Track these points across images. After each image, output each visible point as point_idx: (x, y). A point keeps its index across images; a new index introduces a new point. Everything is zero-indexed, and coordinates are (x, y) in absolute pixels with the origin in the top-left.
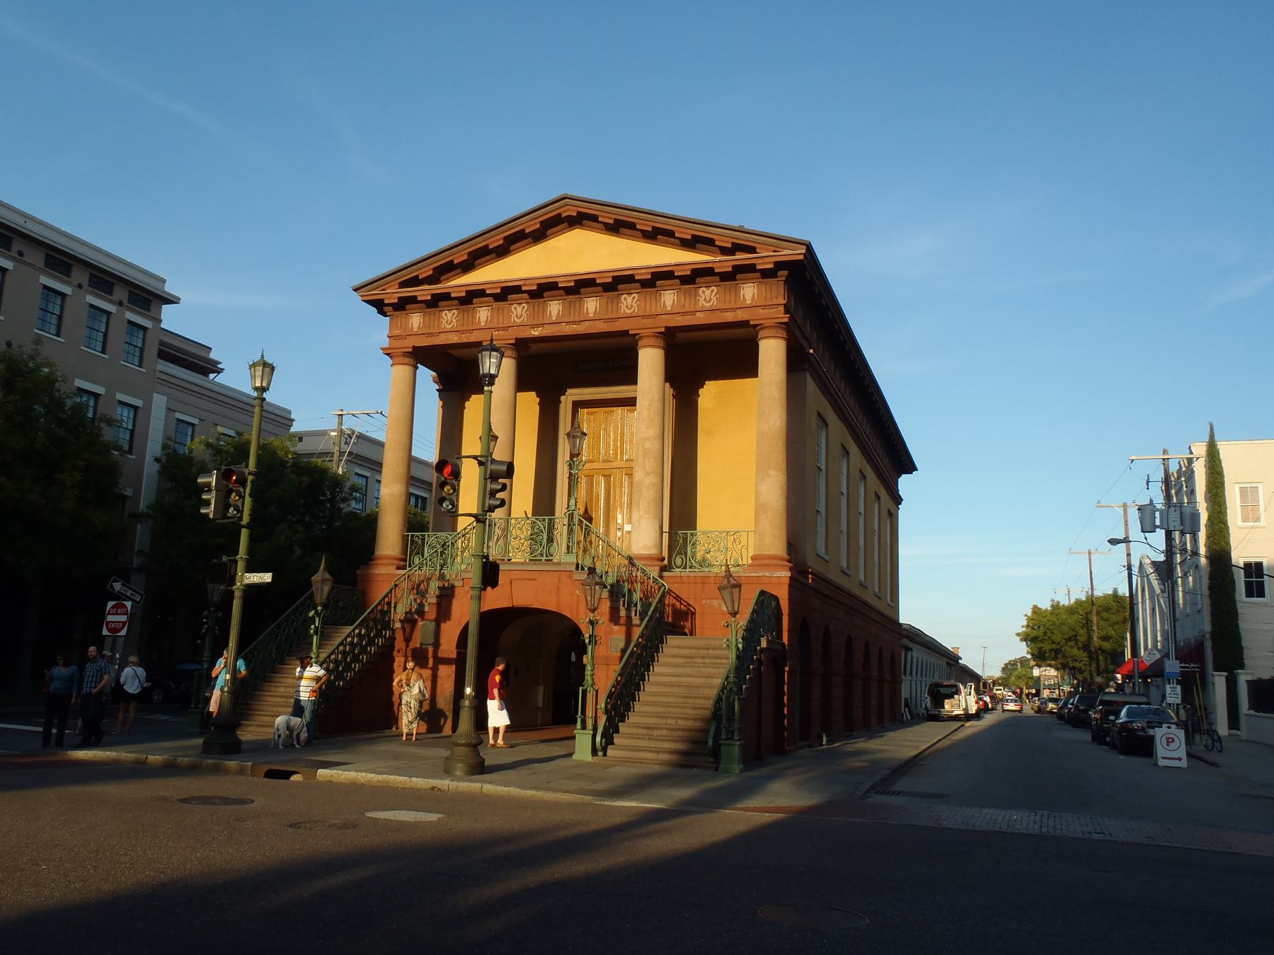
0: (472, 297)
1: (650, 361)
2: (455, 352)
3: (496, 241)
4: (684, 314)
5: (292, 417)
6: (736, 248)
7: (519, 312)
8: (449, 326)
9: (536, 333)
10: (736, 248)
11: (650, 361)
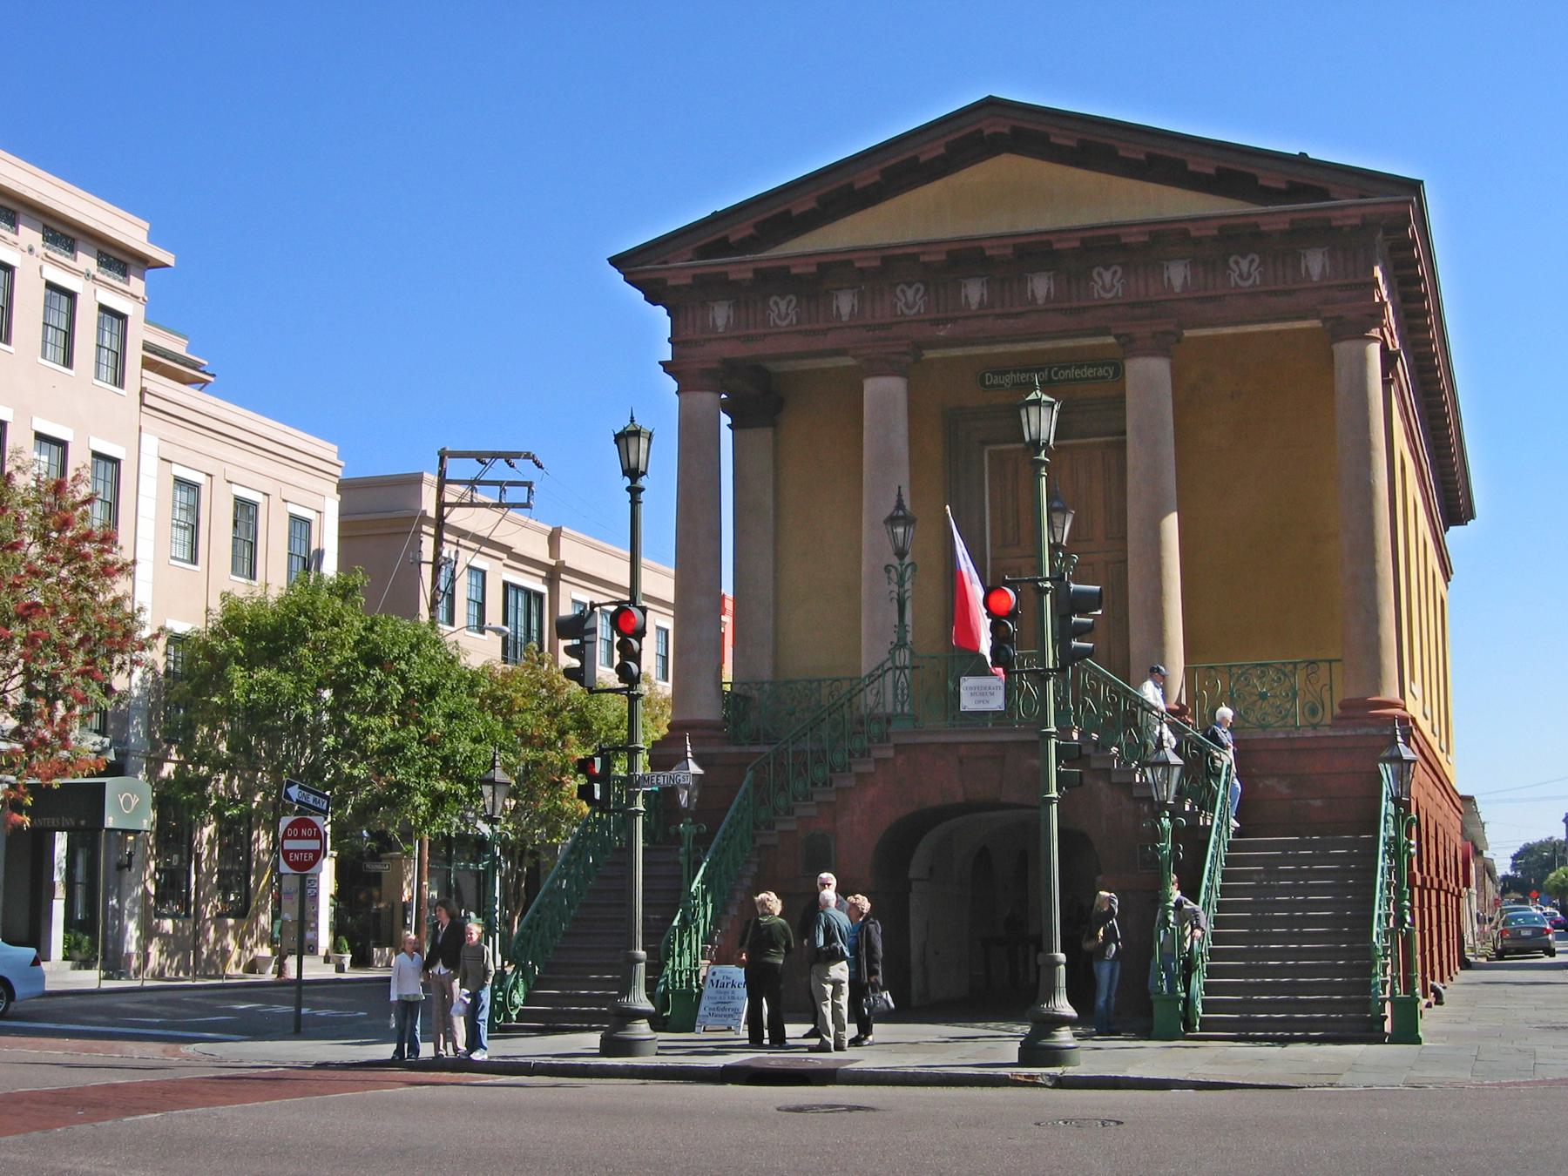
2: (772, 366)
6: (1296, 192)
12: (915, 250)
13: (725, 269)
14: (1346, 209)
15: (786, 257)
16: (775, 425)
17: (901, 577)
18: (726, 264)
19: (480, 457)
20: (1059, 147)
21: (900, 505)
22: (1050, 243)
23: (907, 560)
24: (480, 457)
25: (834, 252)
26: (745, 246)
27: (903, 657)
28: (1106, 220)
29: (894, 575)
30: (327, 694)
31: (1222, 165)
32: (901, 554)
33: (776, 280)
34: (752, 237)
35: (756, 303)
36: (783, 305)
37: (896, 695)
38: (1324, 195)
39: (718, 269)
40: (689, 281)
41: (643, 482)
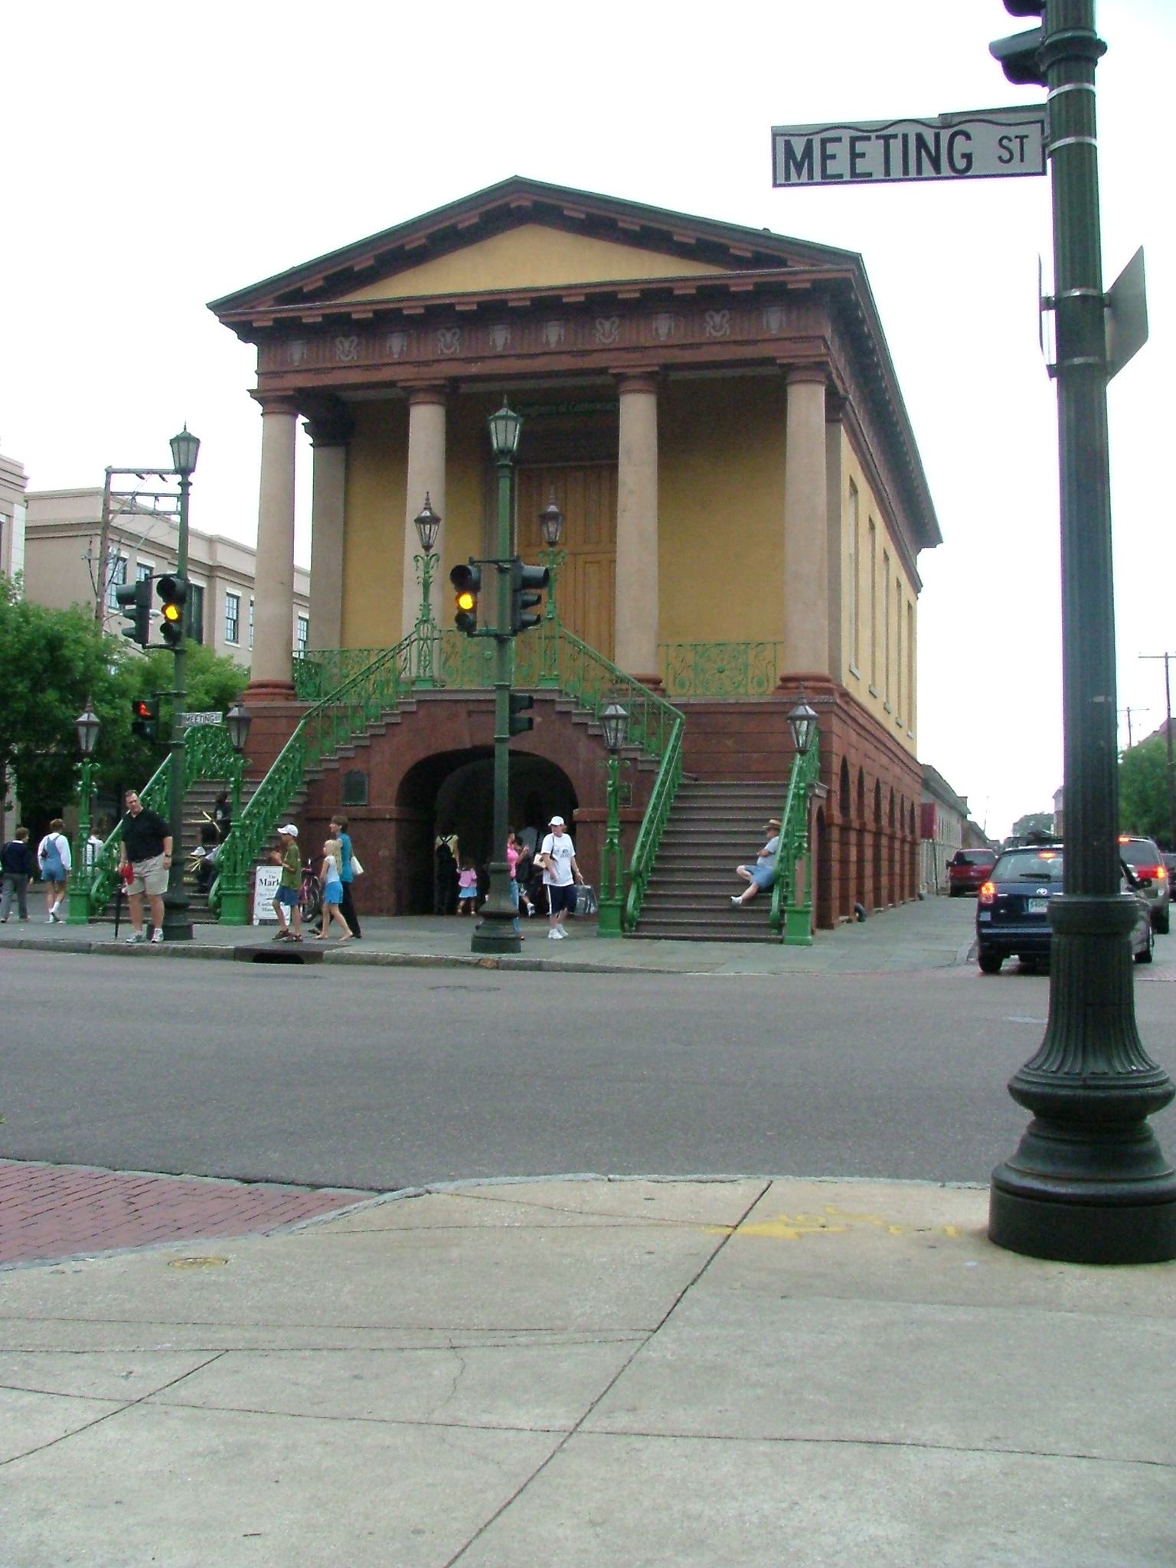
0: (387, 320)
1: (637, 418)
2: (343, 395)
3: (419, 240)
4: (683, 347)
5: (25, 473)
6: (760, 260)
7: (447, 344)
8: (346, 364)
9: (474, 369)
10: (760, 260)
11: (637, 418)
12: (453, 300)
13: (300, 314)
14: (799, 275)
15: (347, 305)
16: (347, 445)
17: (427, 565)
18: (300, 309)
19: (139, 474)
20: (571, 218)
21: (428, 507)
22: (727, 286)
23: (432, 551)
24: (139, 474)
25: (439, 297)
26: (313, 296)
27: (425, 630)
28: (608, 279)
29: (421, 563)
30: (488, 1117)
31: (325, 274)
32: (427, 548)
33: (340, 325)
34: (321, 288)
35: (336, 341)
36: (347, 344)
37: (419, 662)
38: (781, 262)
39: (291, 314)
40: (270, 323)
41: (191, 478)
